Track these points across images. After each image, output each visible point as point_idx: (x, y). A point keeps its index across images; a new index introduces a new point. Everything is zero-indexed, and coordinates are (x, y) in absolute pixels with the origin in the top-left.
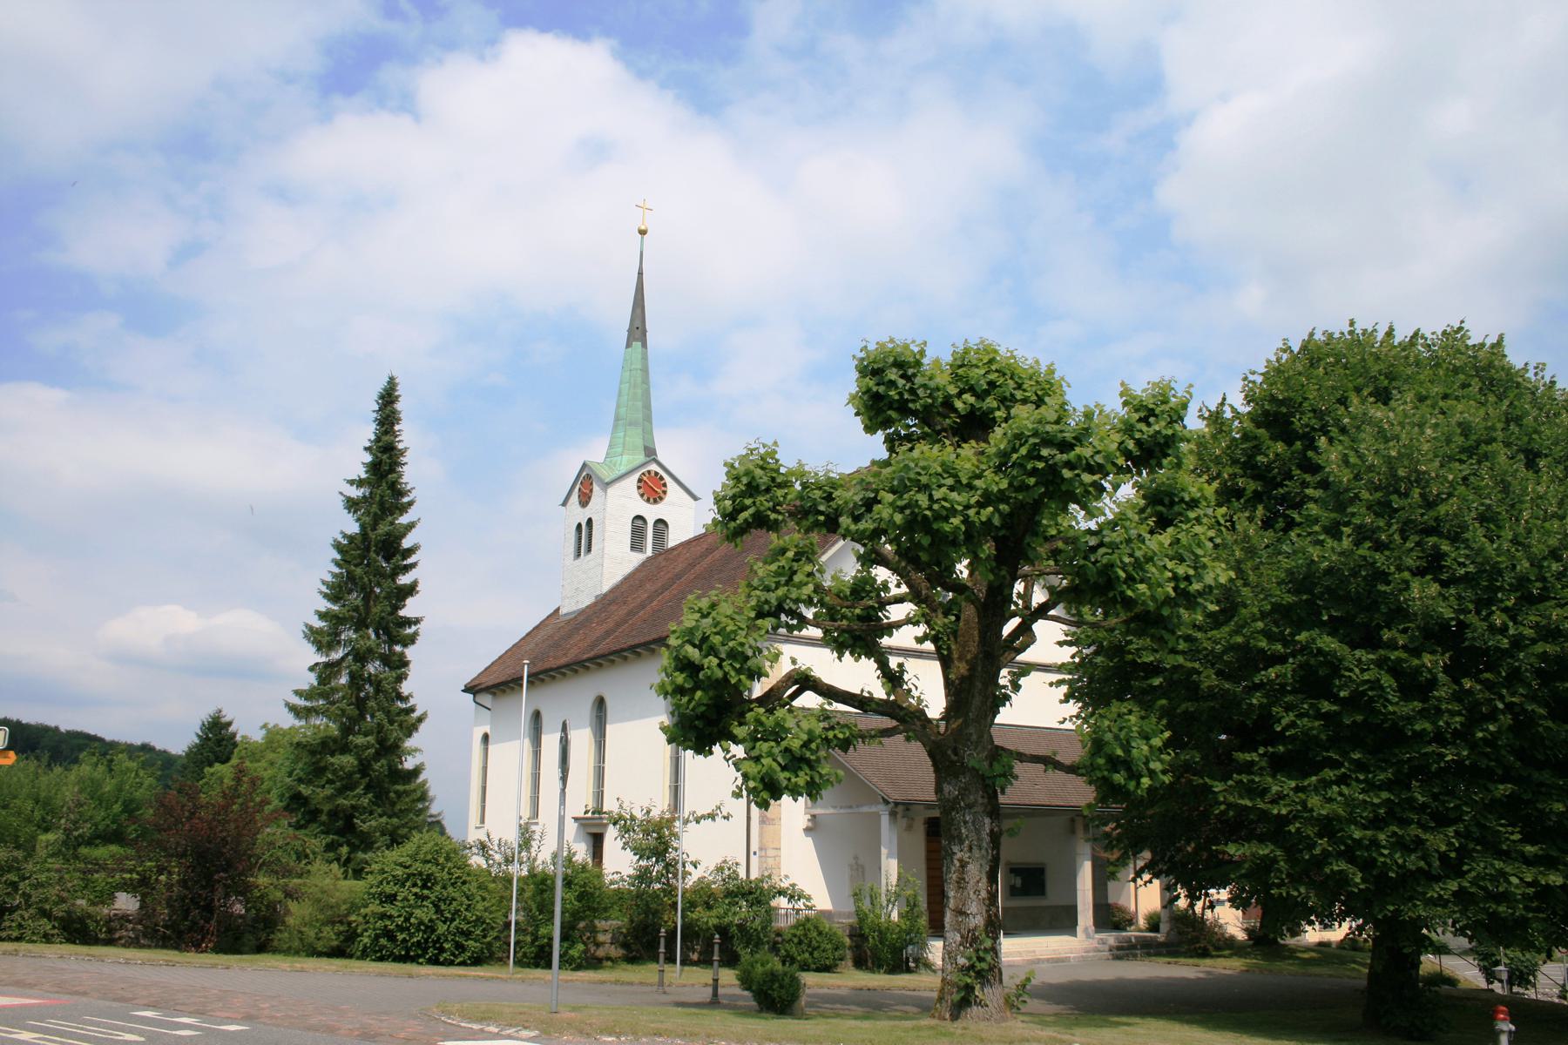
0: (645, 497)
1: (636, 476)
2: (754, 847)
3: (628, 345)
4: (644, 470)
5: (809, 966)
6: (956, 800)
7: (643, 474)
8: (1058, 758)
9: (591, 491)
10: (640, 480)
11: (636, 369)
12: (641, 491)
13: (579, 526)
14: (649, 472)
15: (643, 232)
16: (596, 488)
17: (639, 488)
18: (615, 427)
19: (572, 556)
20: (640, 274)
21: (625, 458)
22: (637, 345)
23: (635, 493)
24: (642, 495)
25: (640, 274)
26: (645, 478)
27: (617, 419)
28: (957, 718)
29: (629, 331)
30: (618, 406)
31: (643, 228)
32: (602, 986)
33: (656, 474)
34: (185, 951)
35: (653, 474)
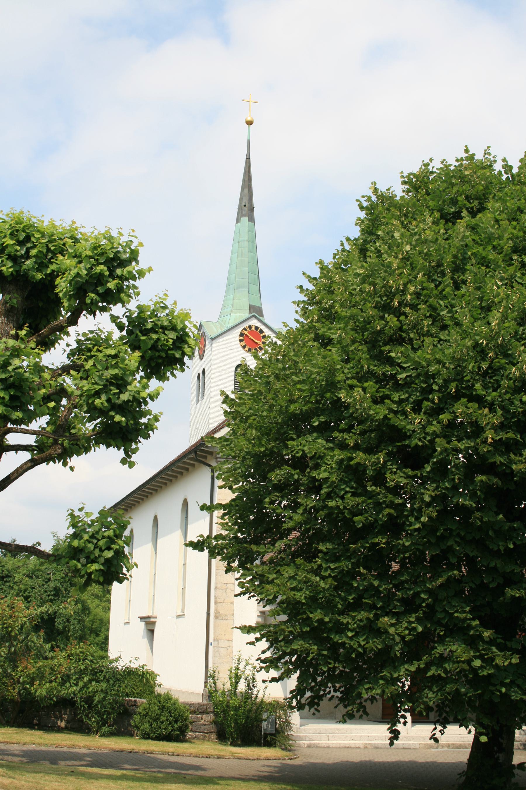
0: (247, 348)
1: (239, 330)
2: (211, 640)
3: (238, 221)
4: (246, 325)
5: (148, 734)
6: (446, 627)
7: (245, 329)
8: (41, 548)
9: (205, 346)
10: (242, 335)
11: (244, 241)
12: (243, 343)
13: (199, 375)
14: (250, 327)
15: (250, 123)
16: (207, 343)
17: (241, 341)
18: (227, 290)
19: (195, 401)
20: (248, 159)
21: (233, 316)
22: (245, 220)
23: (238, 346)
24: (244, 347)
25: (248, 159)
26: (246, 333)
27: (229, 284)
28: (505, 550)
29: (239, 209)
30: (229, 274)
31: (249, 119)
32: (222, 753)
33: (257, 328)
34: (187, 704)
35: (253, 329)
